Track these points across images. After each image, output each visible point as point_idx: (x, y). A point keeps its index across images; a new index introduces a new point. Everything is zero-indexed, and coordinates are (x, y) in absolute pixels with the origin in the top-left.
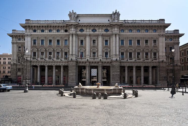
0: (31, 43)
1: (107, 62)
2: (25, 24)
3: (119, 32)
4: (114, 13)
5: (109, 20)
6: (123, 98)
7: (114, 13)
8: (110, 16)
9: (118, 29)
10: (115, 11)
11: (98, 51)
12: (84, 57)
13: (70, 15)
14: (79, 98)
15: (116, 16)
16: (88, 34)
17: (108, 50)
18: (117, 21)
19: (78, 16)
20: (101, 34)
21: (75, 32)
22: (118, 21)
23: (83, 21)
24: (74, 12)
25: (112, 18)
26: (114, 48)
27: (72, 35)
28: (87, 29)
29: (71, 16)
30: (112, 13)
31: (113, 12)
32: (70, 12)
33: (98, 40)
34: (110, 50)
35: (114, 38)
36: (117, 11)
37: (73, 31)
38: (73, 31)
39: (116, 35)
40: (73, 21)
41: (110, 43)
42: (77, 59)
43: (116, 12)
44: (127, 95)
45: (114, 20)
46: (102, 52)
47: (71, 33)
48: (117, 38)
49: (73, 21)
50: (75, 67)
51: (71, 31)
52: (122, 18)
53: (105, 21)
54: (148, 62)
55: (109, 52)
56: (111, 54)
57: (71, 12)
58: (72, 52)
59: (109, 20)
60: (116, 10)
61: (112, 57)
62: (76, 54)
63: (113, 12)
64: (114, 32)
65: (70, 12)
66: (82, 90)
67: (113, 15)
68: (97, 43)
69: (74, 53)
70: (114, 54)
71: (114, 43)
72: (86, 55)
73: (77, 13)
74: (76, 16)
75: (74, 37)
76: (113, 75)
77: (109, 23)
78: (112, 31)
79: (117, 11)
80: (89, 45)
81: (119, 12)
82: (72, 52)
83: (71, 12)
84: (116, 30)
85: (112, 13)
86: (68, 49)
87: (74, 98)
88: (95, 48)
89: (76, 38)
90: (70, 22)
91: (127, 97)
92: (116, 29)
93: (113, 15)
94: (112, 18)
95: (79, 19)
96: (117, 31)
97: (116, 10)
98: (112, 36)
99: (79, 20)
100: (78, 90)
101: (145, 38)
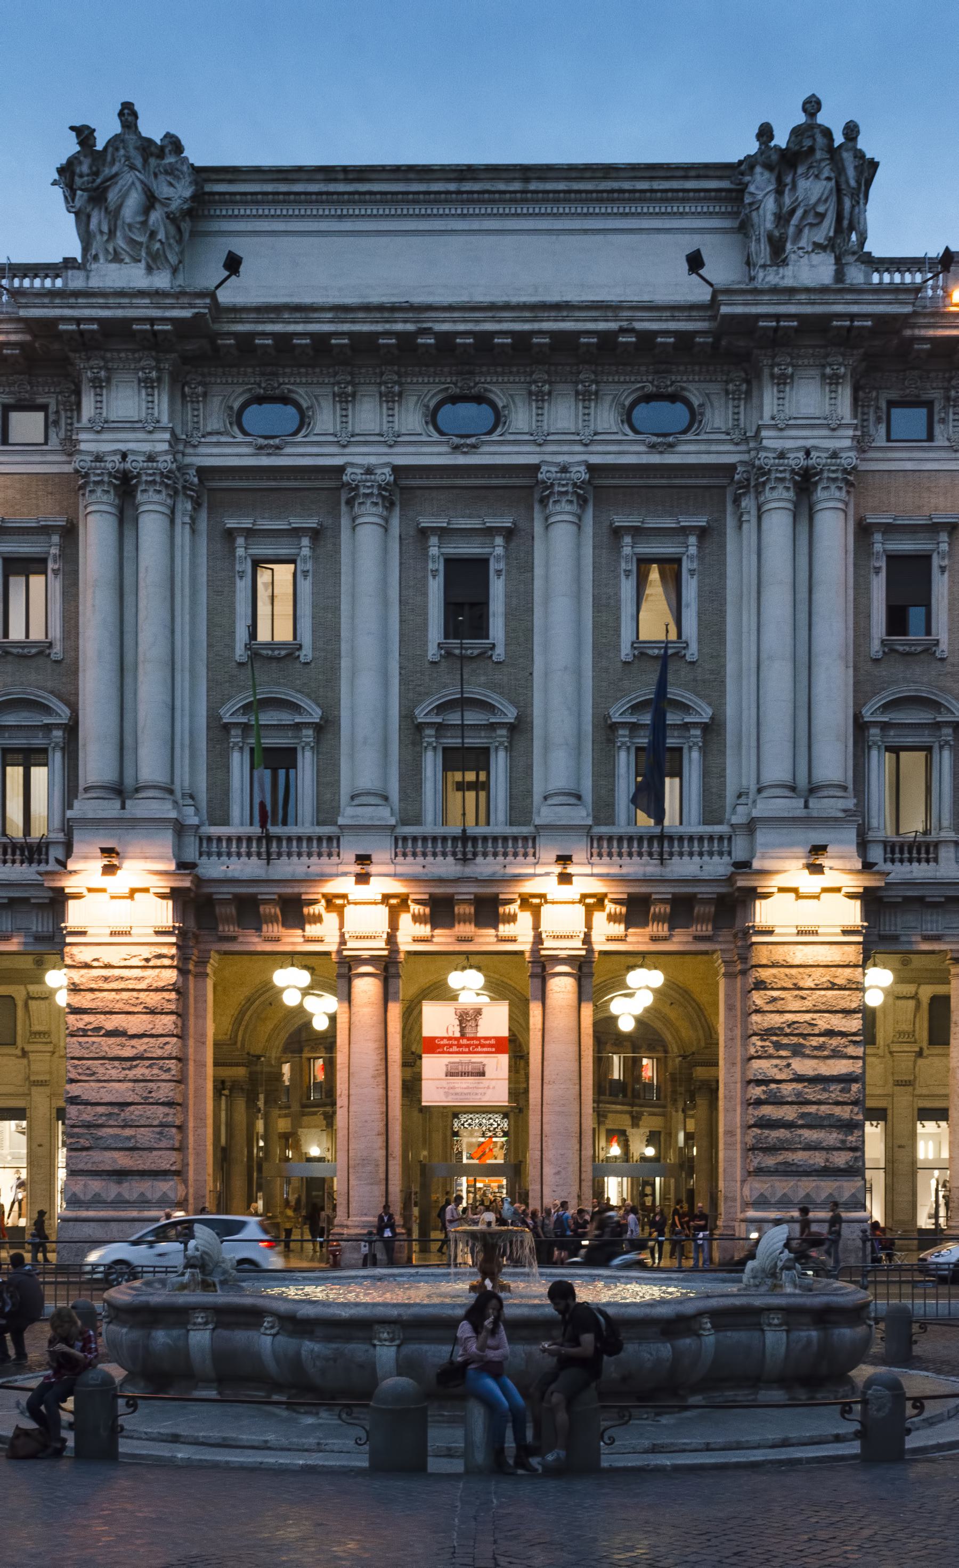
0: (412, 632)
1: (667, 891)
2: (824, 290)
3: (862, 445)
4: (783, 153)
5: (695, 262)
6: (854, 1448)
7: (781, 139)
8: (718, 190)
9: (845, 395)
10: (801, 118)
11: (326, 728)
12: (305, 826)
13: (87, 177)
14: (228, 1468)
15: (812, 188)
16: (369, 471)
17: (685, 708)
18: (811, 269)
19: (214, 198)
20: (385, 475)
21: (160, 444)
22: (839, 275)
23: (292, 272)
24: (152, 128)
25: (744, 228)
26: (778, 679)
27: (125, 487)
28: (345, 399)
29: (98, 196)
30: (753, 147)
31: (765, 133)
32: (84, 134)
33: (523, 568)
34: (74, 708)
35: (778, 525)
36: (821, 119)
37: (132, 426)
38: (132, 426)
39: (805, 483)
40: (134, 276)
41: (722, 614)
42: (191, 854)
43: (810, 134)
44: (919, 1403)
45: (778, 255)
46: (588, 746)
47: (99, 458)
48: (833, 528)
49: (134, 276)
50: (171, 976)
51: (103, 426)
52: (897, 226)
53: (642, 271)
54: (920, 900)
55: (704, 751)
56: (737, 773)
57: (107, 129)
58: (123, 747)
59: (695, 262)
60: (812, 106)
61: (751, 826)
62: (182, 780)
63: (765, 133)
64: (771, 440)
65: (84, 134)
66: (240, 1337)
67: (761, 184)
68: (510, 615)
69: (149, 766)
70: (777, 769)
71: (778, 602)
72: (345, 791)
73: (198, 154)
74: (178, 193)
75: (151, 526)
76: (757, 1092)
77: (703, 295)
78: (749, 423)
79: (821, 119)
80: (384, 638)
81: (852, 131)
82: (123, 747)
83: (107, 129)
84: (807, 413)
85: (753, 147)
86: (54, 703)
87: (868, 1459)
88: (475, 692)
89: (183, 535)
90: (76, 281)
91: (911, 1442)
92: (125, 402)
93: (761, 184)
94: (744, 228)
95: (239, 246)
96: (148, 426)
97: (812, 106)
98: (748, 503)
99: (233, 264)
100: (161, 1337)
101: (889, 529)
